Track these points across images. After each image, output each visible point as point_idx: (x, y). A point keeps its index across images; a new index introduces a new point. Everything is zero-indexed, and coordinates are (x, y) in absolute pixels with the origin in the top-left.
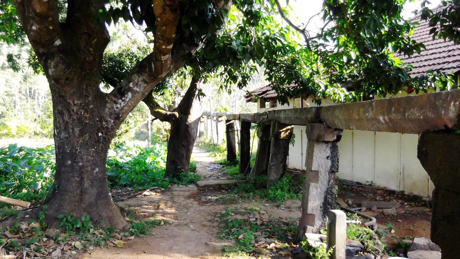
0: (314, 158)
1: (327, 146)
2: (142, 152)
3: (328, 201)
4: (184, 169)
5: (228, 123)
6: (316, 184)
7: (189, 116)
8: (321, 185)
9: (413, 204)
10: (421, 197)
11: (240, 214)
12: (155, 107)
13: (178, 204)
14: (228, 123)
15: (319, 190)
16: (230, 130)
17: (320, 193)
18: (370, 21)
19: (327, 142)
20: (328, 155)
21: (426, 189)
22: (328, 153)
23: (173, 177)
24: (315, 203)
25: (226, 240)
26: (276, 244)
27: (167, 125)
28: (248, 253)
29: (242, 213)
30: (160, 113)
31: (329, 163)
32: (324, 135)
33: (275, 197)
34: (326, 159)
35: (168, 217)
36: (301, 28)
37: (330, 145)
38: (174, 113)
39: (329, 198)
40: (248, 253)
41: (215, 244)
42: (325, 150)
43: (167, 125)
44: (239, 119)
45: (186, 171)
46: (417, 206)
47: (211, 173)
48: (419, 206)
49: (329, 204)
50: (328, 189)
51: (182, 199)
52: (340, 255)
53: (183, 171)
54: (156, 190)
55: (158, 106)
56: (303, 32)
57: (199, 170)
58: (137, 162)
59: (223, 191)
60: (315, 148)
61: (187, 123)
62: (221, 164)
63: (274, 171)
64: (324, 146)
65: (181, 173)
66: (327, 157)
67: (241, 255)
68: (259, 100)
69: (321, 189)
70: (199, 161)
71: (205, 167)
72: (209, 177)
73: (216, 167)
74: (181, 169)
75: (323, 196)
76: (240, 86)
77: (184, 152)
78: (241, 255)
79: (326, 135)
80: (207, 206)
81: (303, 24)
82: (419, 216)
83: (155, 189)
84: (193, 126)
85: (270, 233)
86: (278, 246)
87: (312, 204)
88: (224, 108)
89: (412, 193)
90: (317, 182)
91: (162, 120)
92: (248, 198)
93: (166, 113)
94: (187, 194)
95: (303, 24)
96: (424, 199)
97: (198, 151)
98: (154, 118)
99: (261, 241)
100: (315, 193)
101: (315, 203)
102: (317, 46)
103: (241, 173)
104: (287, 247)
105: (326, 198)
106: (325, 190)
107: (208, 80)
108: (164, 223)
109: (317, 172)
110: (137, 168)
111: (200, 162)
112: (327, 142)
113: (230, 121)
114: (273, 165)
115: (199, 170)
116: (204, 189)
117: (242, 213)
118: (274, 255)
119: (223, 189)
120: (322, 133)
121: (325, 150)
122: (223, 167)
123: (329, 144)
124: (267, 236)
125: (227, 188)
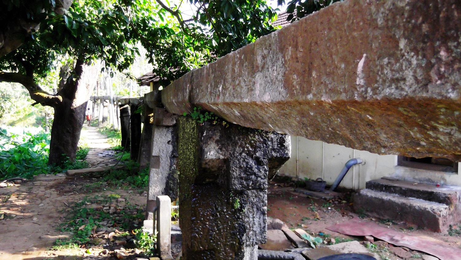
0: (155, 143)
1: (168, 131)
2: (32, 139)
3: (170, 187)
4: (70, 156)
5: (122, 108)
6: (157, 170)
7: (75, 100)
8: (162, 171)
9: (282, 185)
10: (291, 178)
11: (97, 203)
12: (35, 90)
13: (34, 195)
14: (122, 108)
15: (160, 176)
16: (124, 115)
17: (162, 179)
18: (225, 4)
19: (168, 127)
20: (169, 139)
21: (295, 171)
22: (169, 137)
23: (57, 165)
24: (156, 189)
25: (65, 232)
26: (116, 233)
27: (50, 111)
28: (81, 244)
29: (99, 202)
30: (41, 97)
31: (170, 148)
32: (162, 120)
33: (143, 184)
34: (167, 144)
35: (13, 211)
36: (174, 10)
37: (171, 129)
38: (57, 96)
39: (171, 183)
40: (81, 244)
41: (61, 236)
42: (166, 135)
43: (50, 111)
44: (129, 103)
45: (72, 159)
46: (285, 186)
47: (101, 160)
48: (287, 187)
49: (171, 190)
50: (169, 174)
51: (42, 189)
52: (165, 241)
53: (68, 159)
54: (15, 181)
55: (39, 89)
56: (176, 13)
57: (90, 156)
58: (20, 150)
59: (94, 179)
60: (155, 133)
61: (72, 108)
62: (116, 150)
63: (146, 157)
64: (165, 130)
65: (66, 160)
66: (168, 142)
67: (71, 248)
68: (151, 84)
69: (162, 175)
70: (93, 147)
71: (97, 154)
72: (98, 164)
73: (110, 154)
74: (65, 156)
75: (165, 181)
76: (120, 68)
77: (69, 139)
78: (71, 248)
79: (164, 118)
80: (67, 196)
81: (176, 5)
82: (281, 196)
83: (14, 179)
84: (79, 111)
85: (115, 222)
86: (117, 235)
87: (153, 190)
88: (128, 92)
89: (284, 174)
90: (158, 167)
91: (43, 104)
92: (116, 185)
93: (48, 97)
94: (51, 183)
95: (176, 5)
96: (294, 179)
97: (98, 137)
98: (35, 102)
99: (101, 231)
100: (156, 178)
101: (156, 189)
102: (194, 29)
103: (132, 159)
104: (127, 235)
105: (167, 183)
106: (167, 175)
107: (92, 62)
108: (4, 217)
109: (158, 157)
110: (15, 156)
111: (94, 149)
112: (168, 127)
113: (124, 105)
114: (144, 151)
115: (89, 157)
116: (74, 177)
117: (99, 202)
118: (108, 245)
119: (94, 177)
120: (161, 117)
121: (166, 135)
122: (117, 153)
123: (170, 128)
124: (112, 225)
125: (99, 176)
